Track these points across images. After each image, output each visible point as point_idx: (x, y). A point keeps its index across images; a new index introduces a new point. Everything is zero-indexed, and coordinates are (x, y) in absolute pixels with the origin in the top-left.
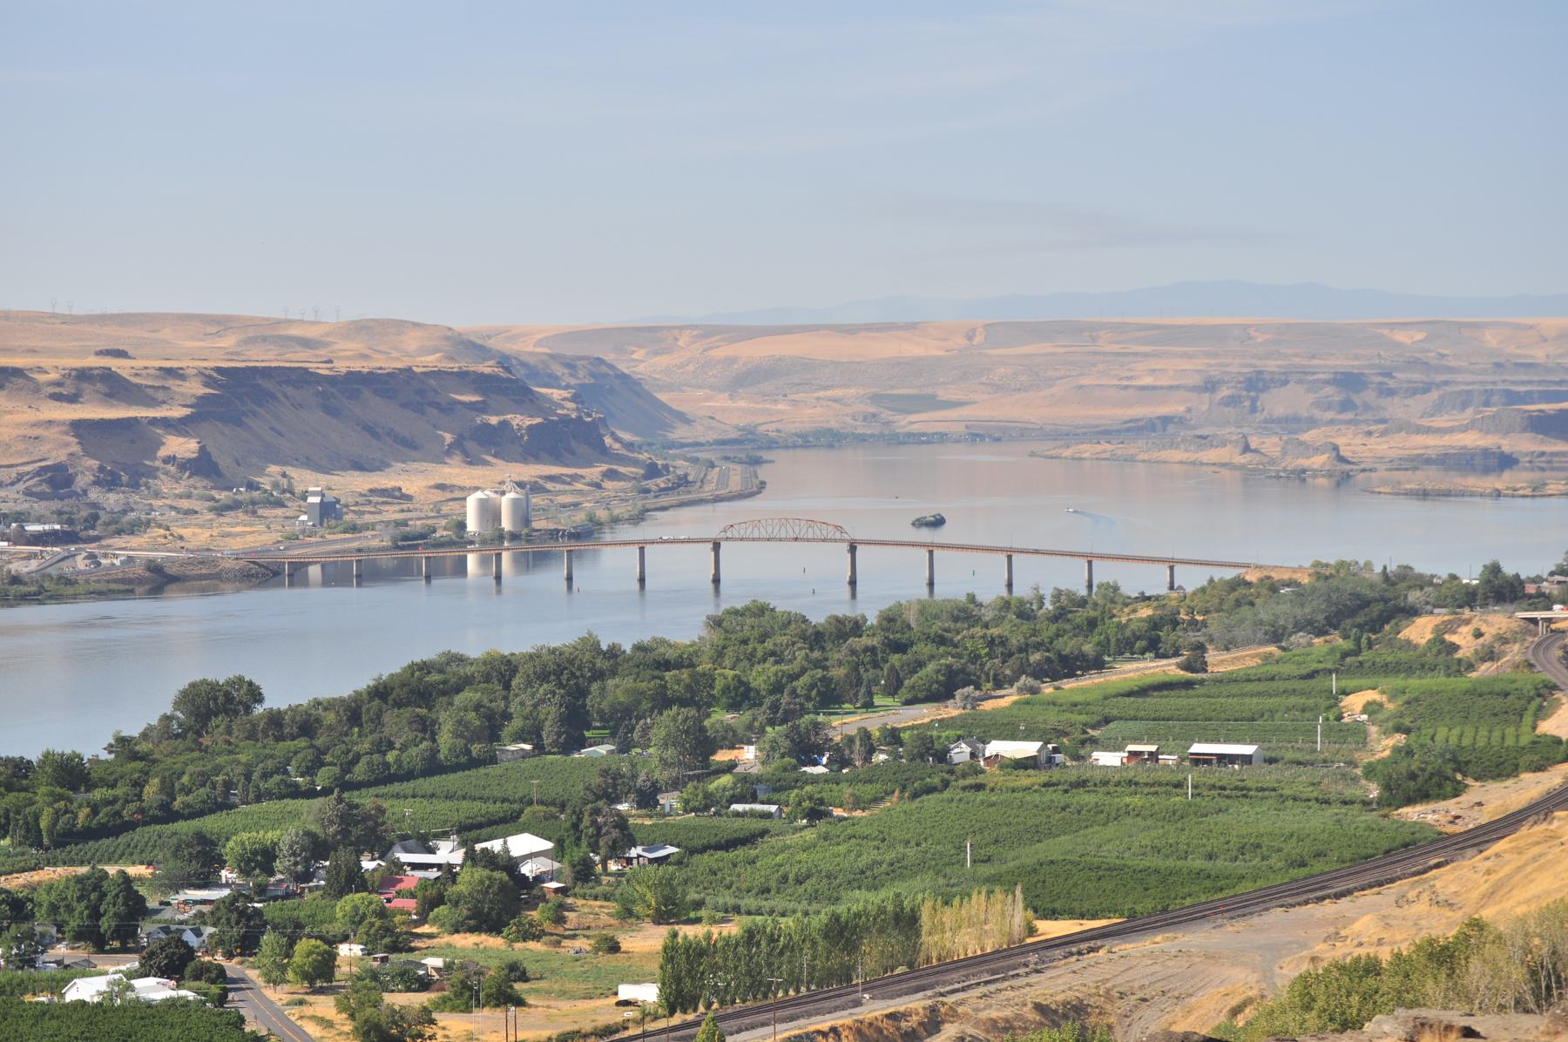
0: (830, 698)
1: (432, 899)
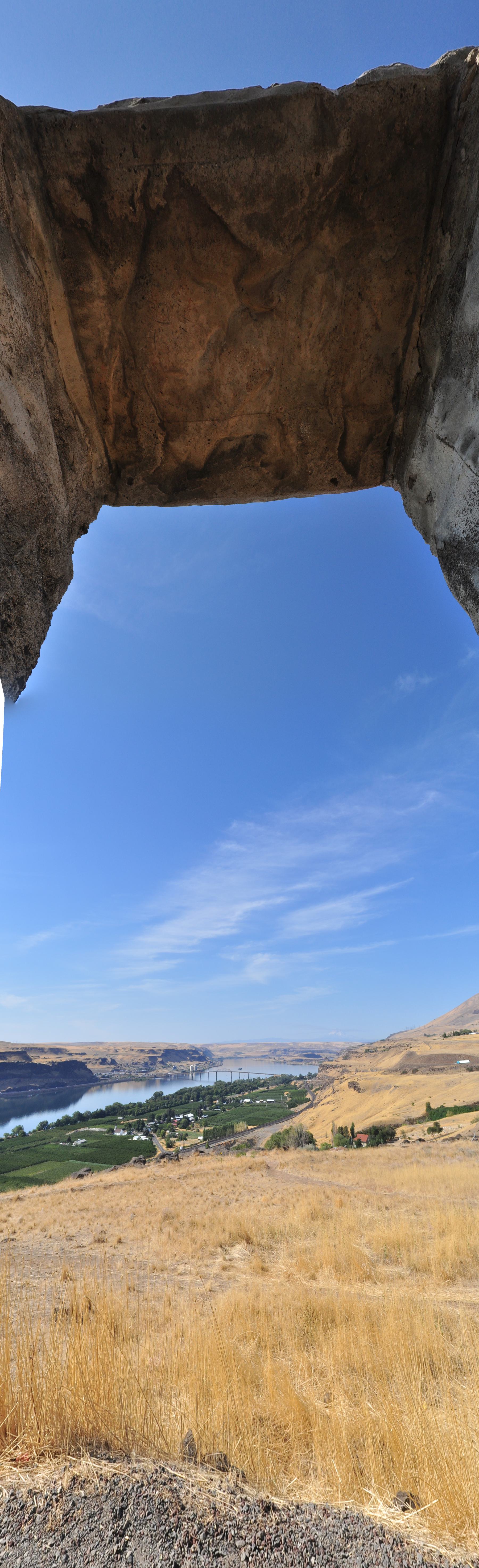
0: (227, 1093)
1: (178, 1123)
